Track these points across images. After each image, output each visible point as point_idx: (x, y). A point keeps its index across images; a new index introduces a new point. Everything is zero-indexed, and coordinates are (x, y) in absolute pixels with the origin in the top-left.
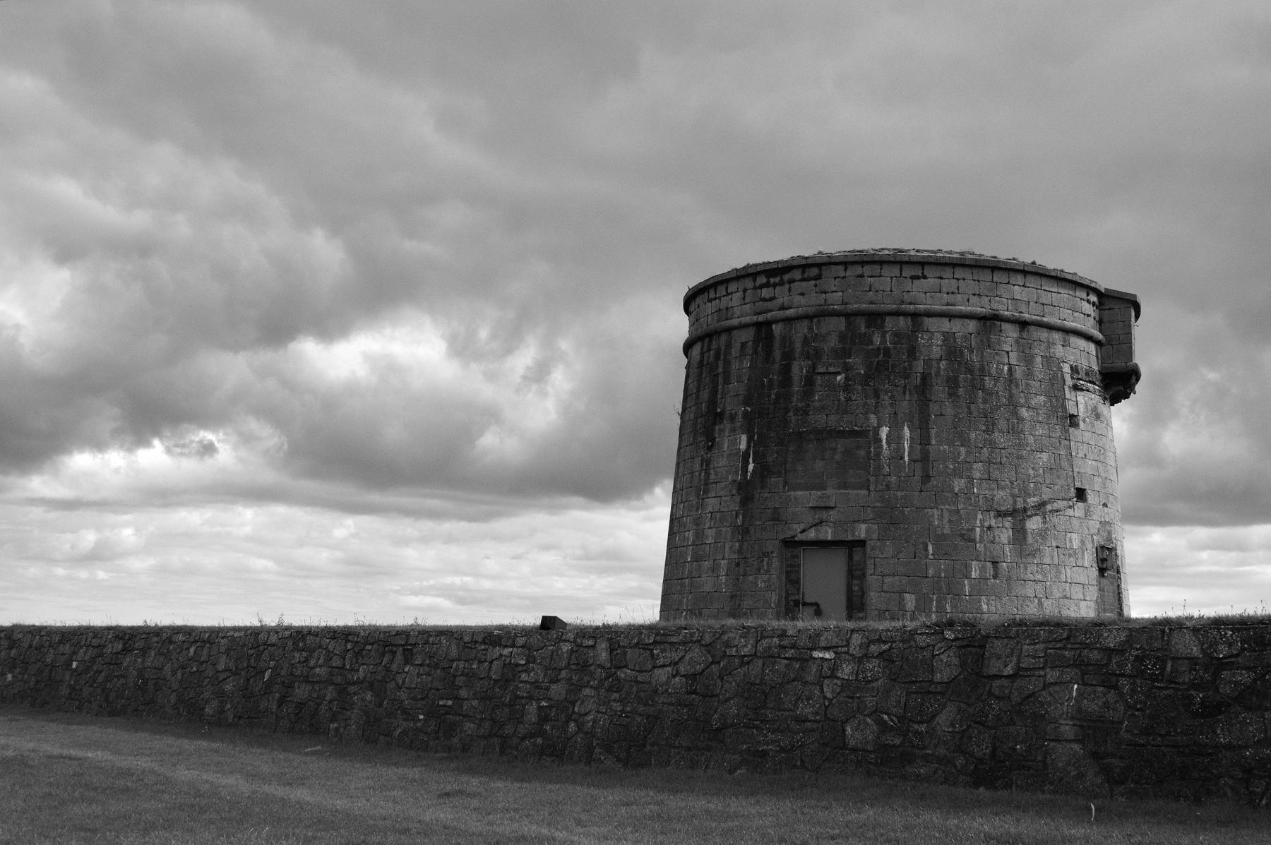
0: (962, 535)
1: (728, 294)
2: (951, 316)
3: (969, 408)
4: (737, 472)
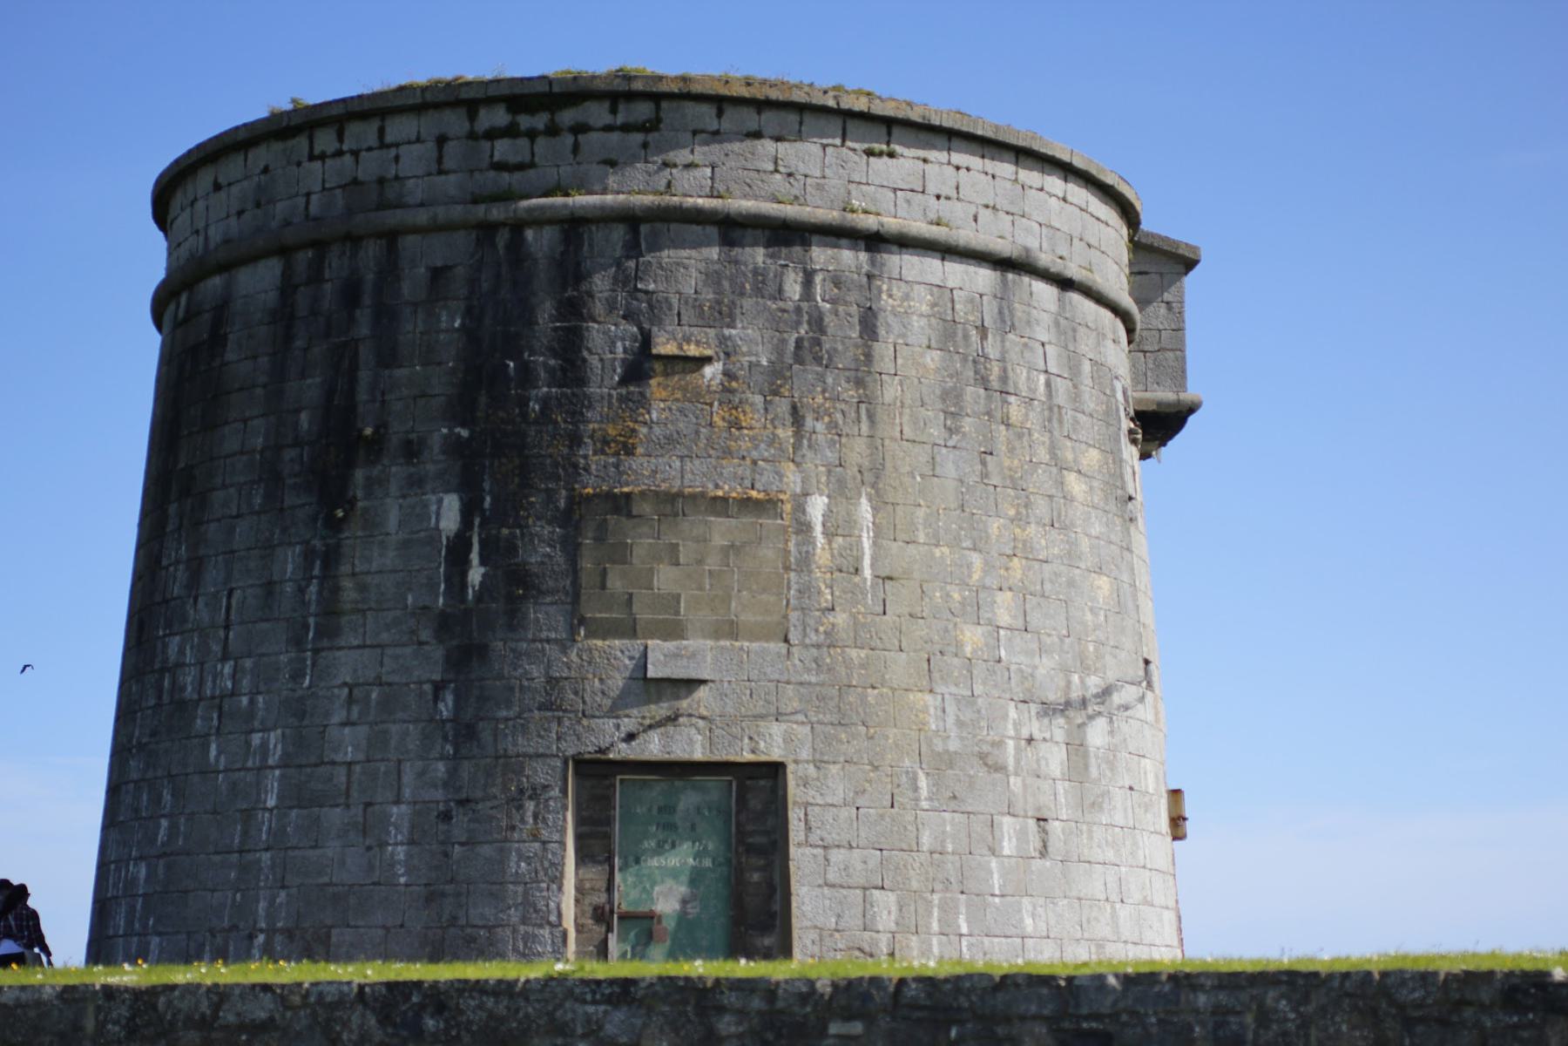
0: (983, 757)
1: (383, 145)
2: (948, 251)
3: (984, 463)
4: (432, 587)
